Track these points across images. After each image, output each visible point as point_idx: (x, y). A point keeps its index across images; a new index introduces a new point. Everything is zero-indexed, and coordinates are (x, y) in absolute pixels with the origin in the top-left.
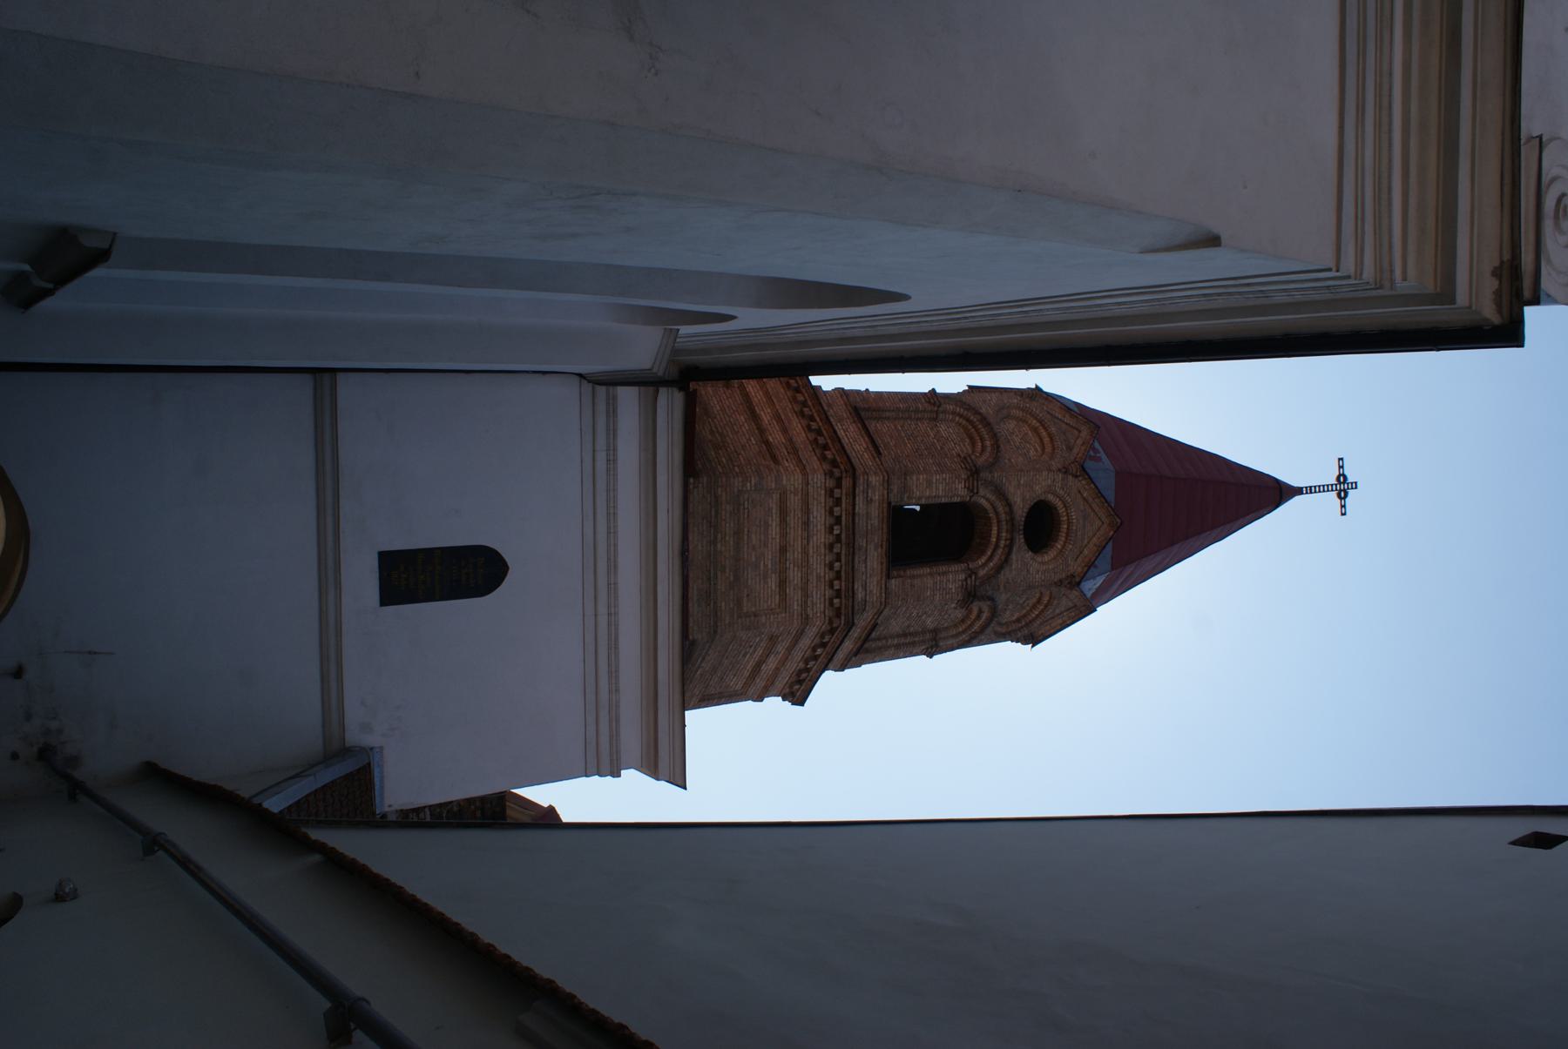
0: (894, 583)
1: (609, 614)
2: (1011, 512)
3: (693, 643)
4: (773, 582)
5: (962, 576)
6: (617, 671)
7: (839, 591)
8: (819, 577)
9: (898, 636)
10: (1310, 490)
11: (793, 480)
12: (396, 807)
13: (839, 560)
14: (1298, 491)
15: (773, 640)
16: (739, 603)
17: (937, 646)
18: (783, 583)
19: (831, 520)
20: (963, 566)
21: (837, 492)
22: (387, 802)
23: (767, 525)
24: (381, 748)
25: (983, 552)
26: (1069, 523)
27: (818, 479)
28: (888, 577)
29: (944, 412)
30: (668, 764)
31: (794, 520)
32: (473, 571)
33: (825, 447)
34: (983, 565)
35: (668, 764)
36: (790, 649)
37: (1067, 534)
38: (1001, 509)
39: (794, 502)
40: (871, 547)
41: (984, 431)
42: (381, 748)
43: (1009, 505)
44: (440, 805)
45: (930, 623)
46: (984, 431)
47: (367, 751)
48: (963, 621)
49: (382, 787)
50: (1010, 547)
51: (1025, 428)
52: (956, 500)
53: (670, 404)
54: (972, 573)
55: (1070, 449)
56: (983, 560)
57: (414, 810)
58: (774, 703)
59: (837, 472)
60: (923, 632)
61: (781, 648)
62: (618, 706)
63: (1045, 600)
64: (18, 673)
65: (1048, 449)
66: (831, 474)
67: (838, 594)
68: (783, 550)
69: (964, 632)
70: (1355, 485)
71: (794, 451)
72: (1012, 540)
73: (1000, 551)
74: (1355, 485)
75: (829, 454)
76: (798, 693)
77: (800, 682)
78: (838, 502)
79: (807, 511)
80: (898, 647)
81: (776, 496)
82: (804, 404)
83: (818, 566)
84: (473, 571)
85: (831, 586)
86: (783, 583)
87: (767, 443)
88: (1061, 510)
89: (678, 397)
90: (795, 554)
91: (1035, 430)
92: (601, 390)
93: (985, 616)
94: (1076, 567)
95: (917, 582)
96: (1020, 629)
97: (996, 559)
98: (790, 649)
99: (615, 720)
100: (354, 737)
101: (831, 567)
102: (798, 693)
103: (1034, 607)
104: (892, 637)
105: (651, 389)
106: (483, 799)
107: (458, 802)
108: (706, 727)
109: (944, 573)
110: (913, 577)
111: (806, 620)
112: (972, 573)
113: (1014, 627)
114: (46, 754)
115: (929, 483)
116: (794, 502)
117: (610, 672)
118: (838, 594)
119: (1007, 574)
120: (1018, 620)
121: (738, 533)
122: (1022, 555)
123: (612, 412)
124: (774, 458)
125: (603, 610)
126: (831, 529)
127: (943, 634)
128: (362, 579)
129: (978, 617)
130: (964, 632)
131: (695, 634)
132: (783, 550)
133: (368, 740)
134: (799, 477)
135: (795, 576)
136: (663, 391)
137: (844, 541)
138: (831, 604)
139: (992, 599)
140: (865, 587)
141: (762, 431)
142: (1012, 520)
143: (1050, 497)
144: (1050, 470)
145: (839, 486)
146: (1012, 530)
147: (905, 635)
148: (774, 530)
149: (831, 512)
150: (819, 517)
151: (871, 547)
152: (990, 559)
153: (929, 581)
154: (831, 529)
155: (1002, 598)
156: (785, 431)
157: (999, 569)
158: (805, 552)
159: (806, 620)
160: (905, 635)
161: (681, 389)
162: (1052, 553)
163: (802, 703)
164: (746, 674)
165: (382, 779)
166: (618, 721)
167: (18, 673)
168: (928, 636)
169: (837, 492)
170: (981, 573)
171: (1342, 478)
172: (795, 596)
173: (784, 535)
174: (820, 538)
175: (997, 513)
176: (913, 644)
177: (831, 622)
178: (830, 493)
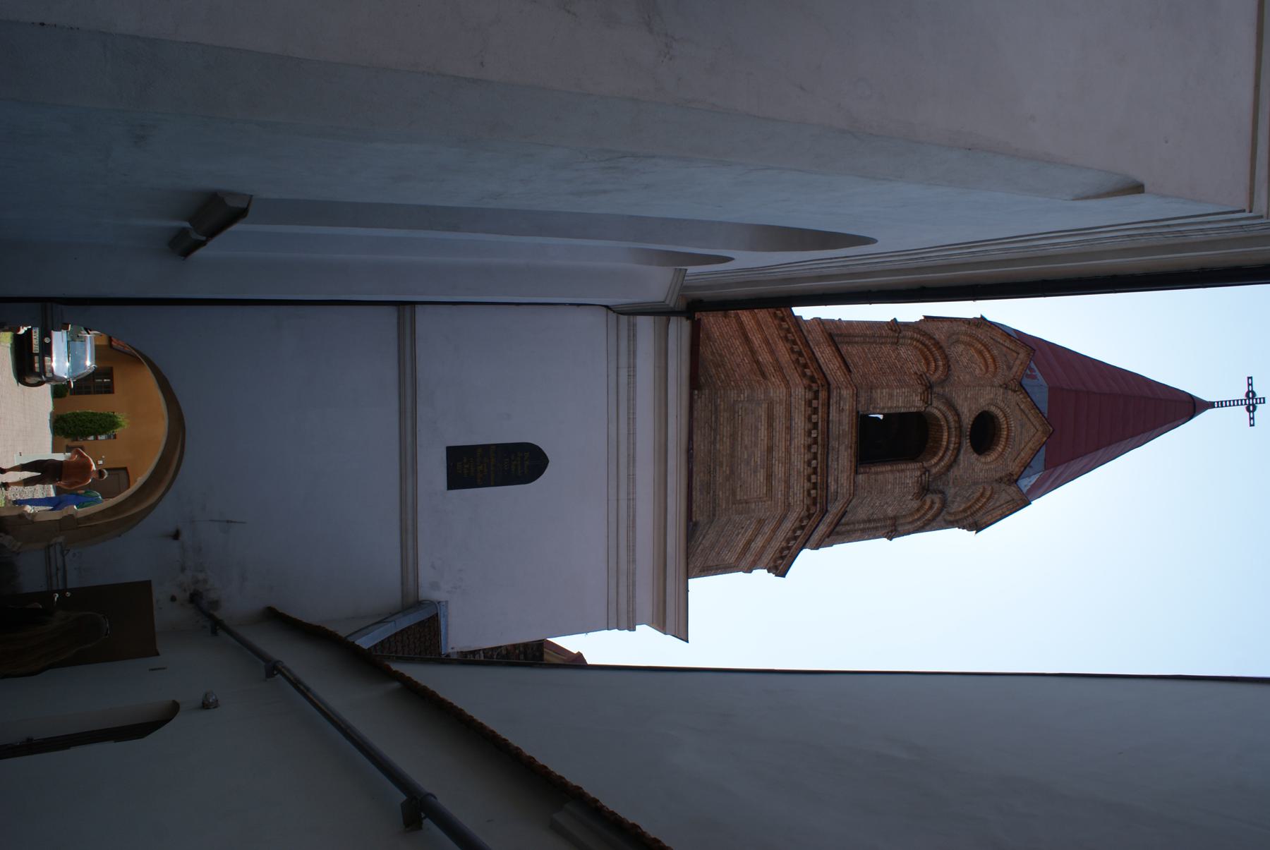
2: (959, 421)
4: (761, 476)
7: (815, 484)
8: (799, 472)
9: (864, 522)
12: (457, 649)
13: (815, 458)
15: (761, 522)
16: (734, 493)
18: (769, 477)
20: (919, 465)
21: (815, 403)
22: (450, 646)
25: (935, 454)
26: (1009, 430)
27: (800, 392)
28: (856, 472)
29: (904, 337)
31: (779, 425)
32: (519, 463)
34: (935, 464)
36: (774, 531)
38: (951, 418)
39: (779, 411)
40: (842, 448)
41: (937, 354)
43: (958, 414)
45: (890, 512)
46: (937, 354)
47: (435, 604)
48: (918, 510)
50: (958, 450)
52: (913, 410)
53: (679, 330)
54: (926, 471)
55: (1010, 368)
58: (761, 575)
59: (815, 387)
60: (885, 519)
61: (767, 530)
62: (634, 574)
63: (988, 493)
64: (176, 536)
65: (991, 368)
66: (810, 388)
67: (815, 486)
68: (770, 450)
69: (918, 519)
70: (1263, 401)
71: (779, 368)
72: (960, 444)
73: (949, 453)
74: (1263, 401)
75: (808, 372)
76: (780, 567)
77: (782, 558)
78: (815, 411)
79: (789, 418)
80: (863, 530)
81: (765, 406)
82: (788, 331)
83: (799, 461)
84: (519, 463)
85: (809, 480)
86: (769, 477)
87: (757, 362)
88: (1002, 419)
89: (686, 325)
90: (779, 453)
91: (980, 353)
92: (624, 319)
93: (937, 506)
94: (1014, 467)
95: (880, 477)
96: (966, 518)
97: (946, 459)
99: (632, 586)
100: (426, 593)
101: (809, 464)
102: (780, 567)
103: (978, 500)
104: (859, 522)
106: (526, 645)
109: (903, 471)
110: (877, 473)
111: (788, 507)
112: (926, 471)
113: (960, 516)
114: (195, 598)
115: (891, 396)
116: (779, 411)
117: (628, 546)
118: (815, 486)
119: (955, 472)
120: (964, 511)
121: (733, 436)
122: (968, 457)
123: (632, 337)
127: (902, 521)
128: (434, 468)
129: (931, 507)
130: (918, 519)
131: (697, 517)
132: (770, 450)
133: (436, 596)
135: (779, 470)
136: (673, 319)
137: (820, 443)
138: (809, 494)
139: (942, 492)
140: (837, 481)
141: (753, 352)
143: (993, 409)
144: (992, 386)
145: (816, 398)
146: (960, 436)
147: (869, 521)
148: (763, 432)
149: (810, 419)
150: (799, 423)
151: (842, 448)
152: (941, 459)
153: (890, 477)
154: (810, 433)
155: (951, 492)
156: (772, 352)
157: (949, 467)
159: (788, 507)
160: (869, 521)
162: (993, 455)
165: (447, 626)
166: (634, 585)
167: (176, 536)
168: (889, 522)
169: (815, 403)
170: (934, 471)
171: (1251, 394)
172: (779, 488)
173: (771, 438)
174: (800, 440)
175: (947, 421)
176: (876, 528)
177: (808, 510)
178: (809, 403)
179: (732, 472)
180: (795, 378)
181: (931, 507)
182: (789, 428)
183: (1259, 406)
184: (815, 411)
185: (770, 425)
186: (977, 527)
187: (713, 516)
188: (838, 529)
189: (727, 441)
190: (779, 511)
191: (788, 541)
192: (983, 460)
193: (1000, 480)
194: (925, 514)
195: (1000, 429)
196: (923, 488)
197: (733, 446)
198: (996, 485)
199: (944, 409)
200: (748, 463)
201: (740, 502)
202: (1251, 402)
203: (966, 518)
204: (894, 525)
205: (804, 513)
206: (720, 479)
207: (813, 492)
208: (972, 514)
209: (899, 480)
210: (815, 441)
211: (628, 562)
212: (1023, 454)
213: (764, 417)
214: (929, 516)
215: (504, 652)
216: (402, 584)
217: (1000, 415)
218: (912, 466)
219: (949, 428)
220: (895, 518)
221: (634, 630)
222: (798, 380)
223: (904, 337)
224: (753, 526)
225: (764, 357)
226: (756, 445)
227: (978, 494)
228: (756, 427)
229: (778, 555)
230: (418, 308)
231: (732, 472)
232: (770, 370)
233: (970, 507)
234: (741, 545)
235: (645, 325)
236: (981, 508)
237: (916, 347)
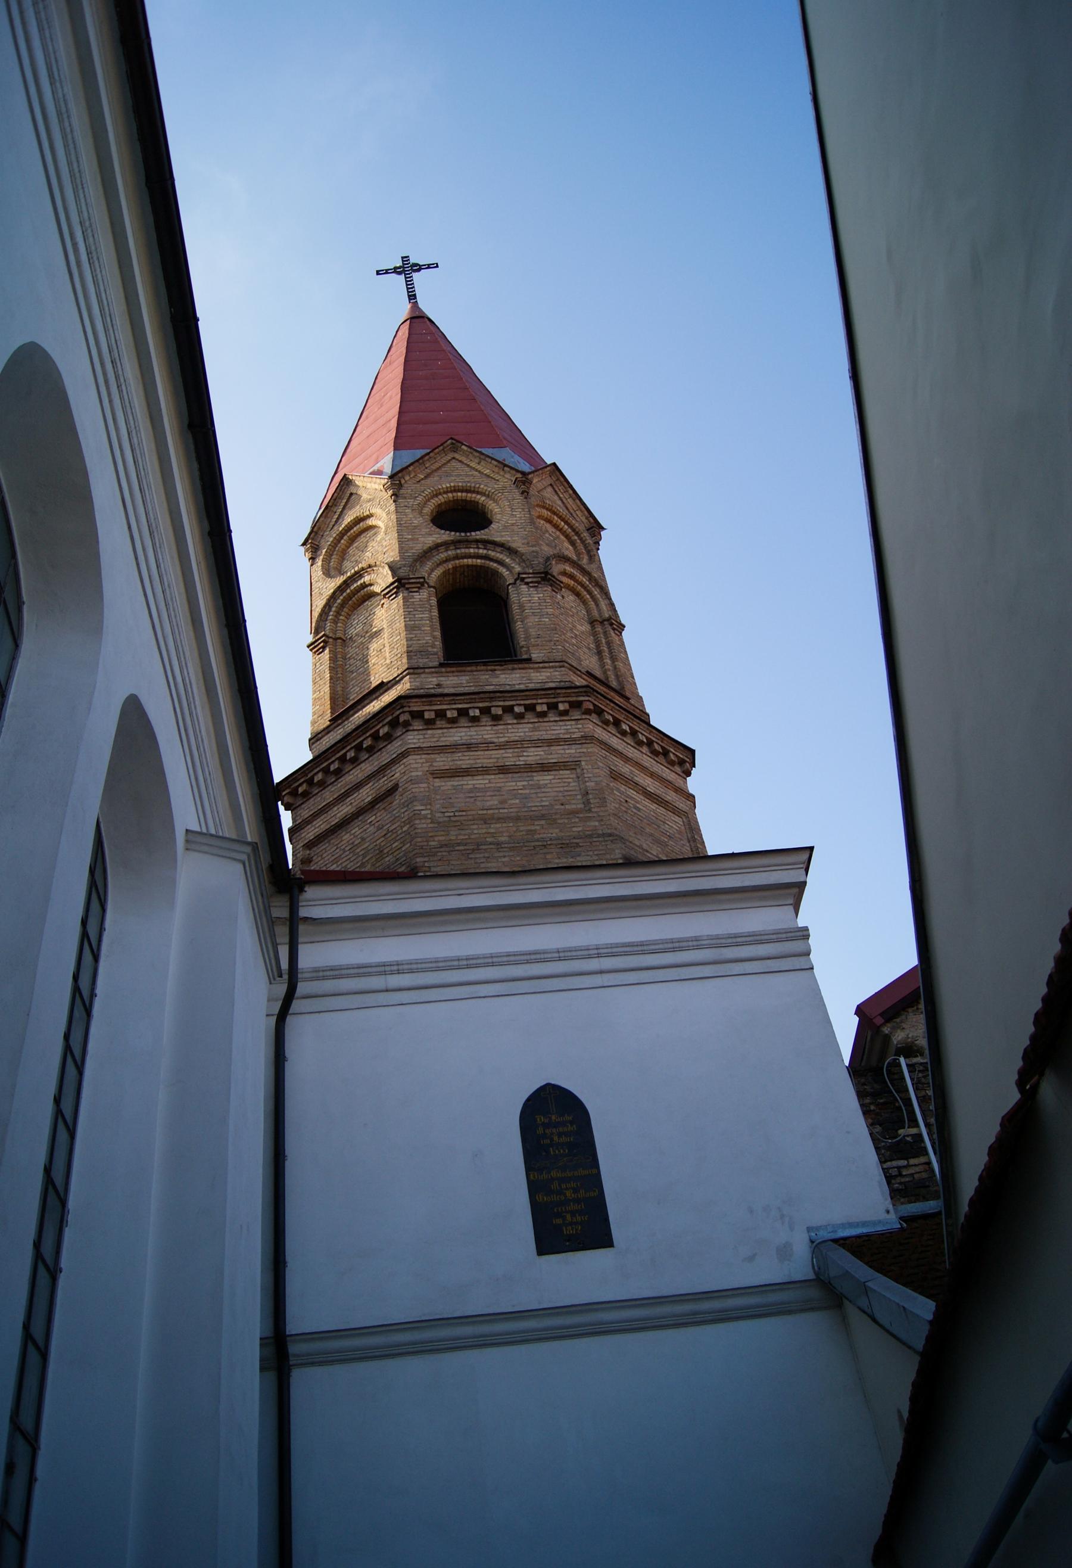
0: (535, 655)
1: (599, 956)
2: (446, 545)
3: (625, 857)
4: (545, 778)
5: (524, 587)
6: (672, 941)
8: (534, 729)
10: (412, 297)
11: (416, 765)
12: (888, 1203)
14: (415, 306)
15: (615, 776)
16: (574, 812)
17: (609, 619)
18: (544, 767)
19: (463, 722)
22: (883, 1216)
23: (475, 789)
24: (809, 1229)
25: (496, 573)
26: (455, 490)
27: (413, 739)
28: (529, 660)
29: (335, 632)
30: (781, 875)
31: (464, 760)
32: (556, 1130)
33: (376, 737)
34: (508, 570)
35: (781, 875)
36: (627, 759)
37: (468, 491)
38: (443, 556)
39: (442, 762)
40: (495, 681)
42: (809, 1229)
43: (437, 547)
44: (877, 1149)
45: (585, 627)
47: (817, 1246)
48: (578, 594)
49: (864, 1224)
50: (486, 543)
51: (351, 551)
52: (434, 601)
53: (318, 903)
54: (520, 578)
56: (502, 570)
57: (889, 1183)
58: (693, 784)
60: (595, 634)
61: (626, 769)
62: (717, 937)
63: (545, 513)
66: (407, 724)
67: (553, 707)
68: (503, 770)
69: (590, 593)
70: (405, 259)
72: (477, 541)
73: (492, 553)
74: (405, 259)
76: (683, 758)
77: (666, 753)
78: (441, 714)
79: (453, 748)
80: (614, 659)
81: (438, 783)
84: (556, 1130)
86: (544, 767)
88: (441, 499)
89: (312, 892)
90: (509, 757)
92: (302, 988)
93: (569, 569)
94: (506, 480)
95: (533, 632)
96: (583, 541)
97: (501, 556)
98: (627, 759)
100: (800, 1266)
102: (683, 758)
103: (556, 526)
105: (302, 928)
106: (861, 1095)
107: (870, 1126)
108: (728, 818)
109: (522, 607)
110: (527, 637)
111: (588, 739)
112: (520, 578)
113: (581, 547)
116: (442, 762)
117: (674, 950)
119: (517, 543)
121: (486, 820)
122: (495, 532)
123: (336, 972)
124: (395, 788)
125: (594, 964)
126: (475, 720)
127: (595, 613)
128: (579, 1277)
129: (571, 577)
130: (590, 593)
131: (617, 856)
132: (503, 770)
134: (411, 759)
135: (533, 755)
136: (303, 912)
137: (490, 707)
138: (565, 713)
139: (548, 559)
142: (456, 543)
143: (427, 510)
146: (467, 543)
147: (599, 653)
148: (480, 781)
150: (459, 734)
151: (495, 681)
152: (501, 563)
153: (532, 621)
155: (547, 550)
157: (512, 551)
158: (500, 747)
159: (588, 739)
161: (302, 890)
162: (491, 505)
163: (692, 752)
164: (661, 810)
165: (851, 1225)
166: (736, 936)
168: (599, 629)
171: (396, 271)
172: (558, 754)
173: (485, 771)
174: (486, 732)
175: (447, 560)
177: (588, 712)
178: (430, 723)
179: (542, 817)
180: (394, 749)
181: (571, 577)
182: (469, 747)
183: (412, 261)
184: (441, 714)
185: (467, 772)
186: (596, 528)
187: (613, 837)
188: (614, 684)
189: (494, 827)
190: (594, 749)
191: (640, 743)
192: (499, 517)
193: (525, 493)
194: (582, 585)
195: (456, 501)
196: (544, 579)
197: (500, 820)
198: (533, 501)
199: (429, 565)
200: (526, 797)
201: (587, 803)
202: (407, 269)
203: (583, 541)
204: (602, 623)
205: (594, 718)
206: (554, 832)
207: (561, 707)
208: (577, 534)
209: (532, 610)
210: (485, 711)
211: (698, 948)
212: (487, 472)
213: (456, 782)
214: (585, 580)
215: (878, 1128)
216: (790, 1312)
217: (435, 501)
218: (513, 597)
219: (457, 557)
220: (592, 622)
221: (806, 929)
222: (397, 744)
223: (335, 632)
224: (623, 788)
225: (366, 794)
226: (499, 790)
227: (548, 526)
228: (470, 791)
229: (661, 759)
230: (302, 1318)
231: (542, 817)
232: (383, 783)
233: (567, 536)
234: (654, 806)
235: (311, 956)
236: (566, 523)
237: (348, 617)
